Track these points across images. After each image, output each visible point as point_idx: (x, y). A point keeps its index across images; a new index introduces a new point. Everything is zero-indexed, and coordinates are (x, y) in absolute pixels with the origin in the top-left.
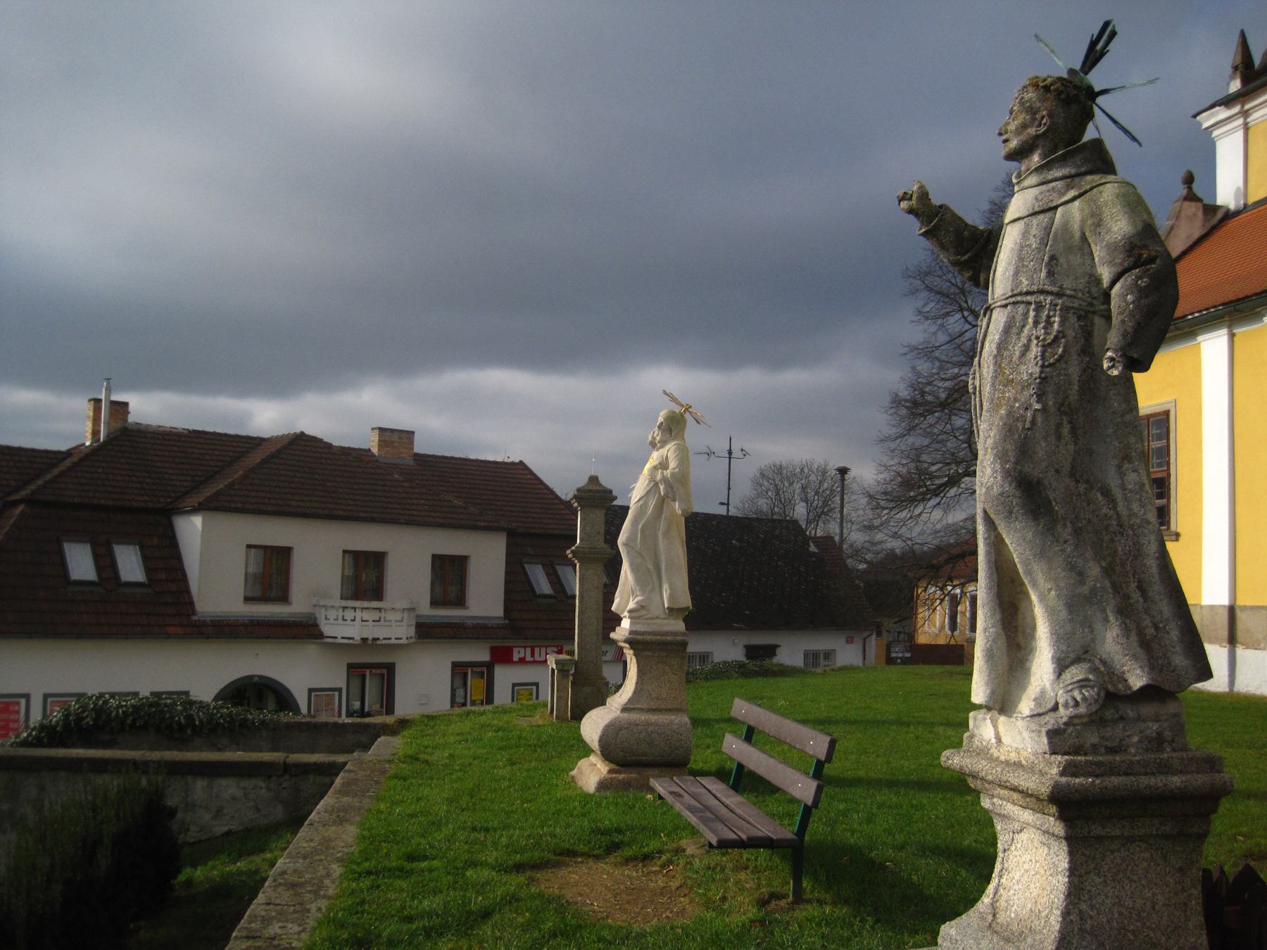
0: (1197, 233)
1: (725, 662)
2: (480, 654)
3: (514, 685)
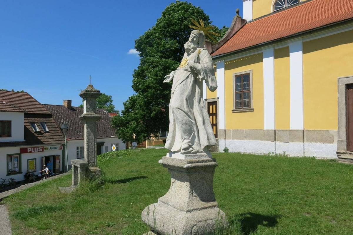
0: (240, 27)
1: (309, 157)
2: (15, 150)
3: (28, 160)
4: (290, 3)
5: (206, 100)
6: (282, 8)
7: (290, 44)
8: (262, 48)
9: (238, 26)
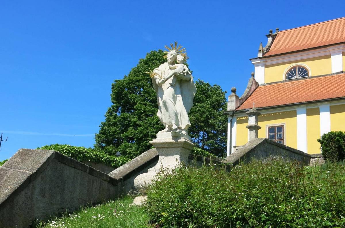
4: (301, 75)
5: (235, 148)
6: (293, 78)
7: (321, 106)
8: (296, 107)
9: (254, 87)
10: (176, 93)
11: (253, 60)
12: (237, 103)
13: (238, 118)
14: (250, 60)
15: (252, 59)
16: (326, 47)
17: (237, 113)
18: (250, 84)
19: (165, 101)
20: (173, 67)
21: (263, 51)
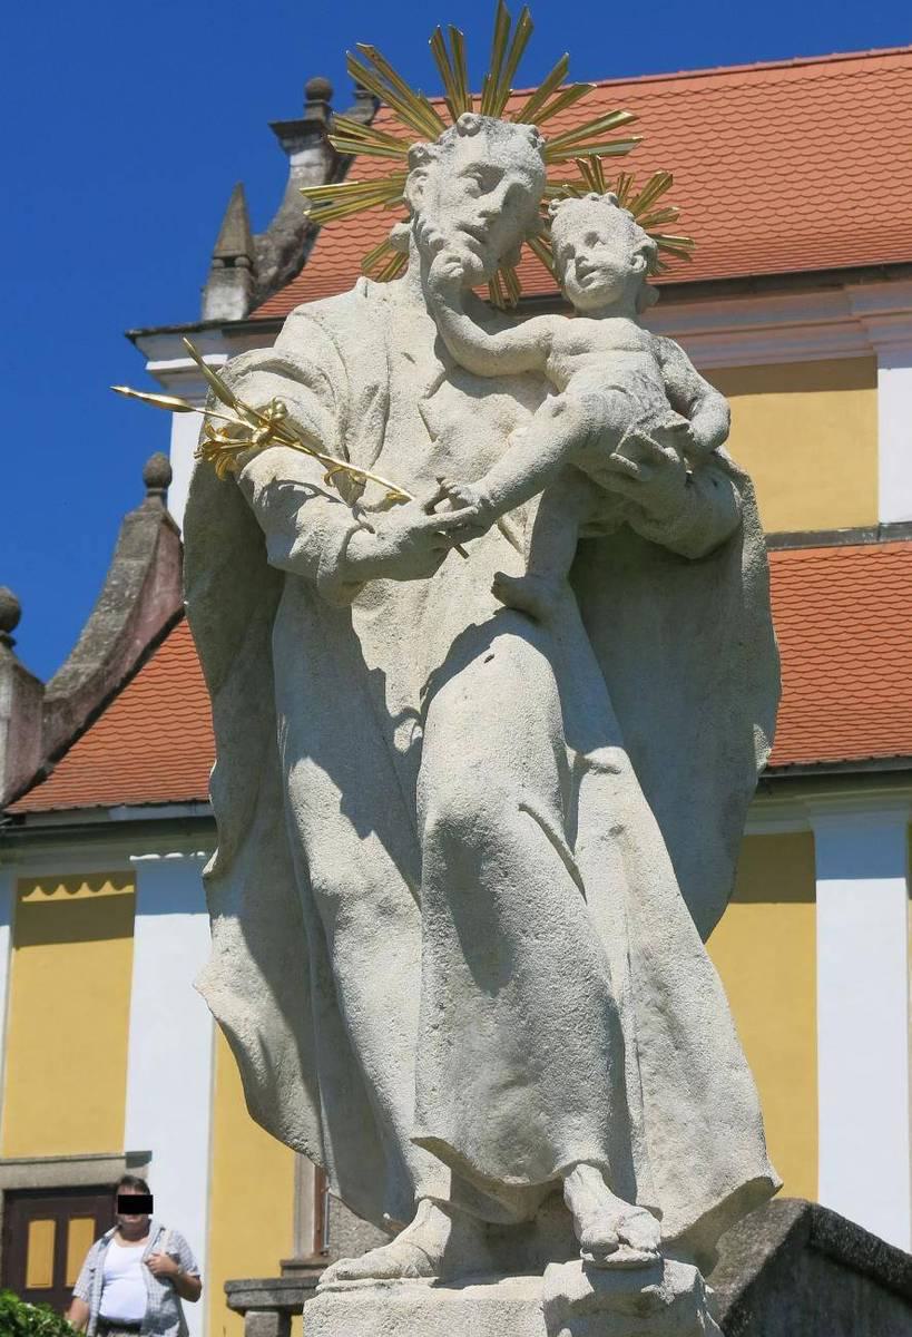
7: (823, 816)
10: (579, 729)
11: (161, 342)
12: (23, 738)
13: (26, 887)
14: (133, 338)
15: (146, 334)
16: (839, 286)
17: (29, 840)
18: (135, 565)
19: (470, 840)
20: (509, 352)
21: (252, 269)
